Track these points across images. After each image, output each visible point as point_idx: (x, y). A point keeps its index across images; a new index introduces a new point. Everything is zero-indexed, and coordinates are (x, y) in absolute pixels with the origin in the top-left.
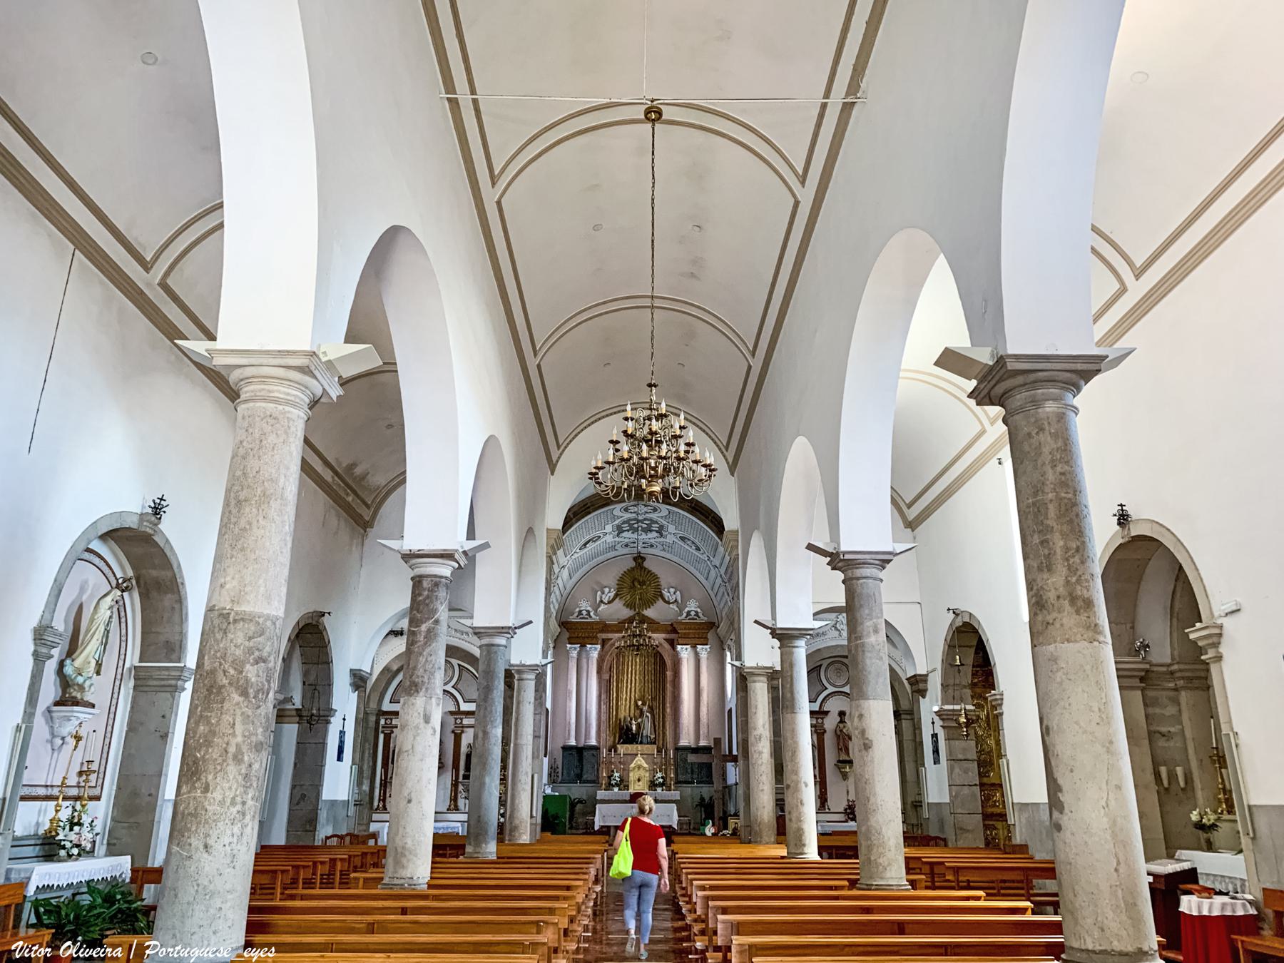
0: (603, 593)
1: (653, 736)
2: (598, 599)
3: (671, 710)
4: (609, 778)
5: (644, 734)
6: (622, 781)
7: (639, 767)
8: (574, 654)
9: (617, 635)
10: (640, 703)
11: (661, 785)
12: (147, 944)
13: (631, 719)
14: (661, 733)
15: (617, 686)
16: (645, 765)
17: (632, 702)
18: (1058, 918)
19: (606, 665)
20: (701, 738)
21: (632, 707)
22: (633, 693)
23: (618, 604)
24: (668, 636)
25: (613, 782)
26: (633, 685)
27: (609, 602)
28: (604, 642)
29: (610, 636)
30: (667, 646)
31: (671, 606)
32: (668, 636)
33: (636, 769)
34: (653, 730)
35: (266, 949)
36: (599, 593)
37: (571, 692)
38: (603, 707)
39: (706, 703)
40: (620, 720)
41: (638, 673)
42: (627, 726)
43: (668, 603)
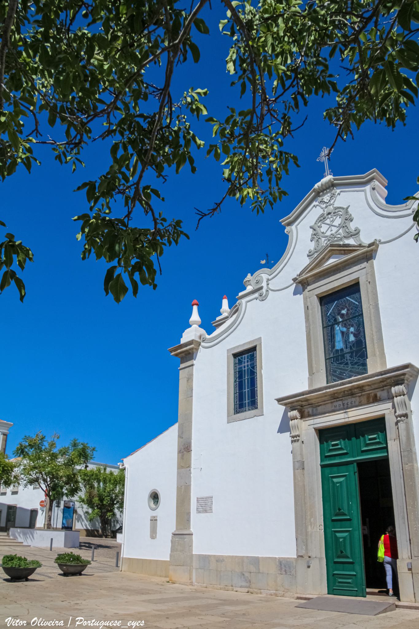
12: (77, 619)
35: (140, 622)
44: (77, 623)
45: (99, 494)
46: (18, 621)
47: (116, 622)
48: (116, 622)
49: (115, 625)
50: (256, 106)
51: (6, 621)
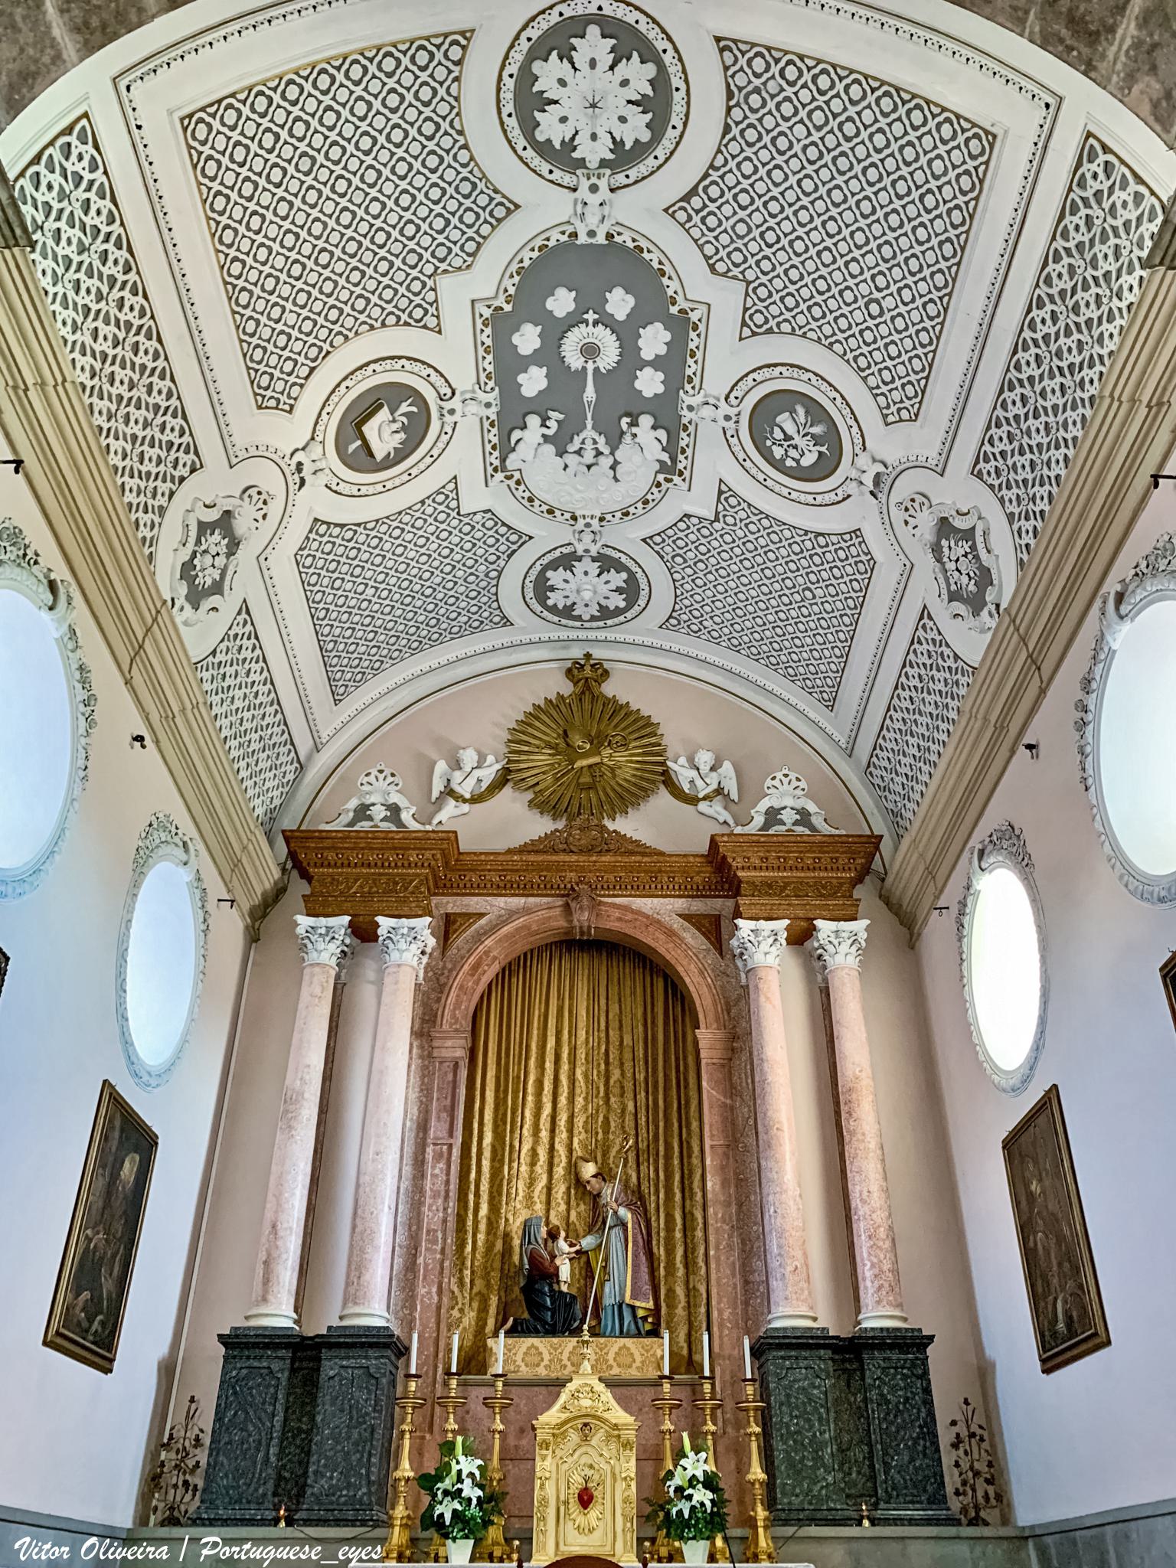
0: (456, 765)
1: (645, 1304)
2: (438, 787)
3: (725, 1183)
4: (427, 1482)
5: (608, 1300)
6: (491, 1501)
7: (586, 1425)
8: (326, 954)
9: (501, 901)
10: (589, 1170)
11: (711, 1523)
12: (203, 1541)
13: (553, 1235)
14: (680, 1291)
15: (499, 1103)
16: (619, 1415)
17: (559, 1171)
18: (151, 1524)
19: (456, 1008)
20: (868, 1294)
21: (560, 1190)
22: (562, 1135)
23: (511, 803)
24: (698, 906)
25: (446, 1509)
26: (563, 1100)
27: (476, 799)
28: (448, 928)
29: (475, 903)
30: (693, 938)
31: (703, 806)
32: (698, 906)
33: (574, 1437)
34: (645, 1276)
36: (441, 767)
37: (290, 1101)
38: (435, 1170)
39: (873, 1144)
40: (507, 1237)
41: (581, 1054)
42: (534, 1258)
43: (693, 800)
44: (205, 1552)
45: (737, 893)
46: (48, 1546)
47: (307, 1548)
48: (307, 1548)
49: (303, 1557)
50: (228, 879)
51: (16, 1546)
